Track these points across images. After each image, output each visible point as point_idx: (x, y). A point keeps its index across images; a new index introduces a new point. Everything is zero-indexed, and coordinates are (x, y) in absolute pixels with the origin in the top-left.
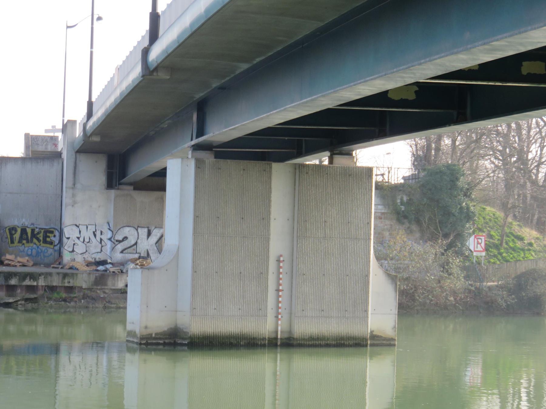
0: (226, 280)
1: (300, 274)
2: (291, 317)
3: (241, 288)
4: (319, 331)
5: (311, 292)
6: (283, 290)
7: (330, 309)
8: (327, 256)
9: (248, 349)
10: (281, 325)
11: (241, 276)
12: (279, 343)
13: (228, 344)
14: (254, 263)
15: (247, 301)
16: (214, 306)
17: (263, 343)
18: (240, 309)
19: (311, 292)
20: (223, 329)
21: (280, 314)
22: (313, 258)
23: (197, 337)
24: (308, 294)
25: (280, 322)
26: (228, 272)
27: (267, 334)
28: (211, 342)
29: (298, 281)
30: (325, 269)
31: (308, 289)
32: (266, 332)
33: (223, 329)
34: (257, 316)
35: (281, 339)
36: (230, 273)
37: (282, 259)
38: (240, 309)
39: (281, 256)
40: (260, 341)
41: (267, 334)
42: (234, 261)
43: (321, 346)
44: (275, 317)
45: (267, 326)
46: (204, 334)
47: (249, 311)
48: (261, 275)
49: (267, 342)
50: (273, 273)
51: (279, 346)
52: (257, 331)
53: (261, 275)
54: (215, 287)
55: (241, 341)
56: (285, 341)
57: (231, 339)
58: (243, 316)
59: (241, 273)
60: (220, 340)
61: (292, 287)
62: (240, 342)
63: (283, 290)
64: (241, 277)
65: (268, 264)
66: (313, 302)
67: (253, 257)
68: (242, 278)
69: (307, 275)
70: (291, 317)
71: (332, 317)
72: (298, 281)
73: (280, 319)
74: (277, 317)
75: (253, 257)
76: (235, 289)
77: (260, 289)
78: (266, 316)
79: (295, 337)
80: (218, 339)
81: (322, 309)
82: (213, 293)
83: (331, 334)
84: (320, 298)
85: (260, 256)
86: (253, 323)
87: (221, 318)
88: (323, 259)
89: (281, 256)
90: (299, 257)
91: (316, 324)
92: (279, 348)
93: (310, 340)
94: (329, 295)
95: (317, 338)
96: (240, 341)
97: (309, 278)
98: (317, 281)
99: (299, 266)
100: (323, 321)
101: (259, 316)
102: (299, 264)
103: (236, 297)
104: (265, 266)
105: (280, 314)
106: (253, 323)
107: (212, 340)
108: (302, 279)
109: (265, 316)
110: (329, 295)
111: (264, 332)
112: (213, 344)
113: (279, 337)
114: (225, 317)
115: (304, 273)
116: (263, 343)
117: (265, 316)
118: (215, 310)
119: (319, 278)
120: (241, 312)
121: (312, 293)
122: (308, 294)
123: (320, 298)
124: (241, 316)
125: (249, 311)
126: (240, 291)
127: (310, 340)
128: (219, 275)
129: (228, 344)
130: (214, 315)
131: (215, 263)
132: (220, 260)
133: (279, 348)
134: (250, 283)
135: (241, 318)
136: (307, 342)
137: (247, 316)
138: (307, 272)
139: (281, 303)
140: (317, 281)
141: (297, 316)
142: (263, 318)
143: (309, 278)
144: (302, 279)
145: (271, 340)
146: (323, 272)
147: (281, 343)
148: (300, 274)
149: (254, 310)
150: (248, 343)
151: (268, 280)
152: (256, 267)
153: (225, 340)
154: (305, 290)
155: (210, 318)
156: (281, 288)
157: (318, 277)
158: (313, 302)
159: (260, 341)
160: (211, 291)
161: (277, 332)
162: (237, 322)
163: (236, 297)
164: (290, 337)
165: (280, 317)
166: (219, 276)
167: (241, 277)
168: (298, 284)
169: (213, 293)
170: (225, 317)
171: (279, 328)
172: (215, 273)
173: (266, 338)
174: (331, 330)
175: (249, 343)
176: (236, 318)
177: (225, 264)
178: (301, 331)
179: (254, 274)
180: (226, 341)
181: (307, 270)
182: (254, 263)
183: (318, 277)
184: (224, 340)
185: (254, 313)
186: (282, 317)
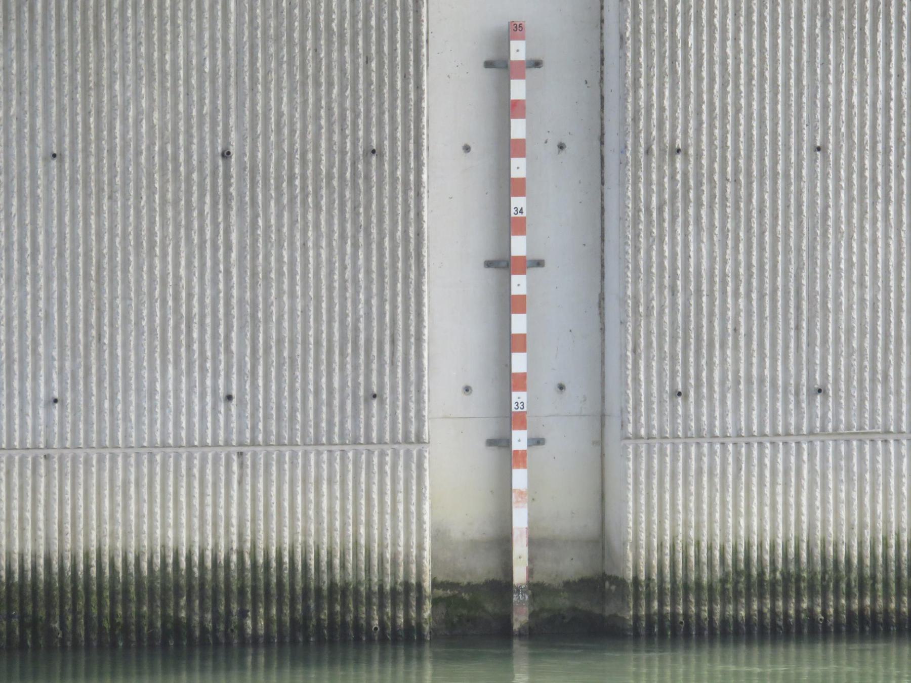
0: (125, 207)
1: (648, 151)
2: (600, 443)
3: (234, 255)
4: (736, 535)
5: (729, 269)
6: (539, 263)
7: (873, 380)
8: (838, 19)
9: (332, 663)
10: (532, 496)
11: (227, 176)
12: (520, 618)
13: (151, 636)
14: (317, 84)
15: (280, 341)
16: (48, 381)
17: (401, 621)
18: (229, 398)
19: (729, 269)
20: (113, 535)
21: (519, 420)
22: (736, 39)
23: (318, 590)
24: (711, 282)
25: (520, 478)
26: (138, 153)
27: (427, 554)
28: (35, 619)
29: (636, 198)
30: (825, 107)
31: (711, 252)
32: (420, 548)
33: (113, 535)
34: (356, 442)
35: (536, 589)
36: (151, 158)
37: (518, 51)
38: (229, 398)
39: (516, 29)
40: (382, 606)
41: (427, 554)
42: (175, 79)
43: (813, 632)
44: (491, 443)
45: (427, 507)
46: (164, 558)
47: (293, 410)
48: (368, 163)
49: (427, 612)
50: (467, 149)
51: (520, 635)
52: (356, 543)
53: (368, 163)
54: (48, 257)
55: (243, 614)
56: (563, 602)
57: (178, 596)
58: (254, 443)
59: (226, 155)
60: (95, 611)
61: (603, 240)
62: (235, 618)
63: (539, 263)
64: (227, 185)
65: (418, 87)
66: (749, 335)
67: (309, 44)
68: (233, 190)
69: (698, 156)
70: (600, 443)
71: (887, 432)
72: (636, 198)
73: (520, 459)
74: (501, 443)
75: (309, 44)
76: (189, 264)
77: (368, 259)
78: (419, 440)
79: (630, 575)
80: (81, 603)
81: (811, 377)
82: (35, 299)
83: (886, 546)
84: (798, 308)
85: (355, 35)
86: (325, 488)
87: (101, 460)
88: (812, 37)
89: (516, 29)
90: (635, 31)
91: (774, 483)
92: (519, 647)
93: (737, 594)
94: (862, 285)
95: (786, 576)
96: (235, 608)
97: (711, 171)
98: (775, 192)
99: (636, 99)
100: (824, 460)
101: (368, 441)
102: (636, 80)
103: (202, 317)
104: (393, 100)
105: (519, 420)
106: (325, 488)
107: (42, 613)
108: (661, 184)
109: (406, 440)
110: (862, 285)
111: (407, 546)
112: (50, 632)
113: (520, 575)
114: (126, 457)
115: (679, 143)
116: (401, 621)
117: (406, 440)
118: (679, 143)
119: (787, 176)
120: (240, 416)
121: (736, 275)
122: (711, 282)
123: (798, 308)
124: (241, 444)
125: (293, 410)
126: (228, 272)
127: (737, 594)
128: (74, 171)
129: (151, 636)
130: (48, 446)
131: (39, 92)
132: (74, 71)
133: (519, 647)
134: (293, 223)
135: (240, 454)
136: (718, 608)
137: (280, 443)
138: (698, 130)
139: (523, 349)
140: (775, 192)
141: (637, 436)
142: (396, 454)
143: (711, 171)
144: (661, 184)
145: (466, 596)
146: (813, 130)
147: (532, 615)
148: (648, 151)
149: (330, 405)
150: (293, 620)
151: (419, 195)
152: (329, 109)
153: (133, 607)
154: (687, 257)
155: (22, 461)
156: (519, 246)
157: (775, 163)
158: (749, 335)
159: (382, 606)
160: (22, 283)
161: (504, 543)
162: (215, 485)
163: (202, 317)
164: (604, 577)
165: (519, 440)
166: (73, 182)
167: (227, 185)
168: (636, 221)
169: (35, 299)
170: (126, 457)
171: (520, 519)
172: (45, 159)
173: (419, 586)
174: (887, 521)
175: (299, 626)
176: (204, 460)
177: (112, 98)
178: (667, 538)
179: (317, 162)
180: (139, 616)
181: (699, 124)
182: (317, 84)
183: (775, 163)
184: (126, 608)
185: (330, 423)
186: (536, 442)
